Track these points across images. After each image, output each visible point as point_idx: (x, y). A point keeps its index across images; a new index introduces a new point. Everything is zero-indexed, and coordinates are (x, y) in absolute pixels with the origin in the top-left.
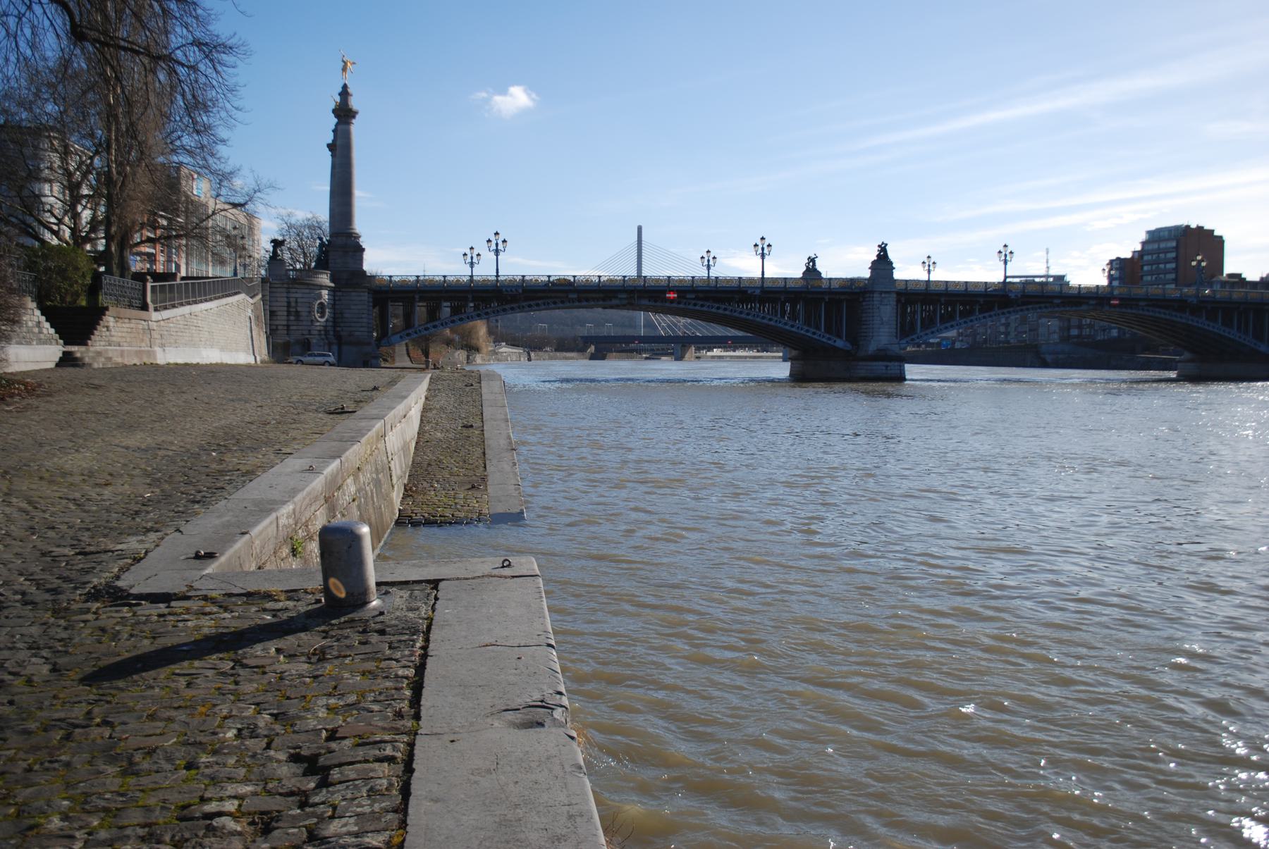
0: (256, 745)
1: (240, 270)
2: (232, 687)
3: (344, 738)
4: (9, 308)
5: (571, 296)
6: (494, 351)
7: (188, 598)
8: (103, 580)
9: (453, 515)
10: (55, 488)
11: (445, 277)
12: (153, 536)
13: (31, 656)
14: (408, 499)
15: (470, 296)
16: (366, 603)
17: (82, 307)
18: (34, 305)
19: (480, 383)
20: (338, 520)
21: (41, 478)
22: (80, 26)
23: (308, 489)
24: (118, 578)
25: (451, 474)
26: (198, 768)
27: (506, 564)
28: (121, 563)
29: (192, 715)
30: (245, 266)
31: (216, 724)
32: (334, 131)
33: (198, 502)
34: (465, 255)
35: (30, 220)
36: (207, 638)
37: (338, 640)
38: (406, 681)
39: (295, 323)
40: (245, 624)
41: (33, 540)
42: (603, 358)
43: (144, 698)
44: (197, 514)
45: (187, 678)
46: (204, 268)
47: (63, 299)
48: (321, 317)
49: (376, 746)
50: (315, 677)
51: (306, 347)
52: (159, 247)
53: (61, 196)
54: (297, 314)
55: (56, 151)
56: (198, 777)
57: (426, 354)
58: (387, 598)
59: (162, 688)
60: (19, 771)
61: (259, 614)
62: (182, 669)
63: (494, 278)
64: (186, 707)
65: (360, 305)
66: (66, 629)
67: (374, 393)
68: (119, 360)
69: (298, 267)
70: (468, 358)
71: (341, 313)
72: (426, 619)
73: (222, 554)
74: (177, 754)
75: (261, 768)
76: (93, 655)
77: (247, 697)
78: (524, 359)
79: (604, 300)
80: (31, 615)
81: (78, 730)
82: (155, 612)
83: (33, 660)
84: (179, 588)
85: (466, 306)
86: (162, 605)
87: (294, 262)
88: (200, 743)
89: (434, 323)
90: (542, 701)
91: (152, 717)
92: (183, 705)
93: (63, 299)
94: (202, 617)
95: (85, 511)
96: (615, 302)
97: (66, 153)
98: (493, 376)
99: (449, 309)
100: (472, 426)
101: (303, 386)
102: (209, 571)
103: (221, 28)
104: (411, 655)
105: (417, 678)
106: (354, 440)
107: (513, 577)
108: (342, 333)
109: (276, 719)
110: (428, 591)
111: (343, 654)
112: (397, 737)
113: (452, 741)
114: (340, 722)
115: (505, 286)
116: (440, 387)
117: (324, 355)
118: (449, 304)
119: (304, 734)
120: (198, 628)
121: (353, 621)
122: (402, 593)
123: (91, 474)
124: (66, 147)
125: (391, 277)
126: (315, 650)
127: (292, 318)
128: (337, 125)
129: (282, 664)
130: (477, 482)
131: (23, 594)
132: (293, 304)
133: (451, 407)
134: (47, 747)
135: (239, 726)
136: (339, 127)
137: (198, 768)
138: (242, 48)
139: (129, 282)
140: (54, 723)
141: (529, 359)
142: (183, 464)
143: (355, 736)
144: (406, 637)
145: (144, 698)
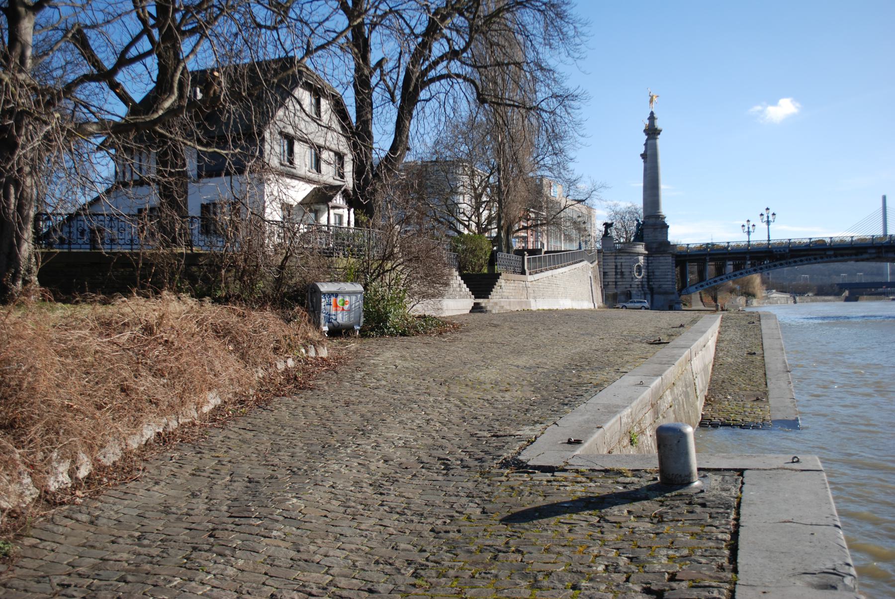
0: (620, 578)
1: (583, 245)
2: (599, 535)
3: (682, 580)
4: (444, 276)
5: (829, 253)
6: (767, 296)
7: (566, 470)
8: (510, 455)
9: (743, 420)
10: (475, 392)
11: (728, 243)
12: (539, 427)
13: (469, 502)
14: (708, 407)
15: (748, 256)
16: (690, 483)
17: (485, 274)
18: (457, 273)
19: (760, 321)
20: (664, 422)
21: (467, 385)
22: (482, 95)
23: (640, 398)
24: (519, 454)
25: (740, 389)
26: (580, 589)
27: (795, 460)
28: (521, 443)
29: (574, 552)
30: (586, 242)
31: (590, 560)
32: (646, 145)
33: (567, 404)
34: (743, 226)
35: (452, 219)
36: (580, 500)
37: (671, 508)
38: (724, 544)
39: (620, 280)
40: (604, 492)
41: (465, 426)
42: (856, 300)
43: (542, 537)
44: (567, 413)
45: (569, 526)
46: (559, 244)
47: (473, 270)
48: (639, 275)
49: (706, 589)
50: (657, 534)
51: (628, 296)
52: (529, 231)
53: (469, 203)
54: (622, 273)
55: (467, 175)
56: (581, 595)
57: (715, 300)
58: (706, 481)
59: (553, 531)
60: (467, 577)
61: (614, 485)
62: (565, 519)
63: (767, 242)
64: (569, 546)
65: (666, 266)
66: (489, 485)
67: (681, 328)
68: (508, 308)
69: (622, 241)
70: (747, 302)
71: (653, 272)
72: (736, 498)
73: (586, 441)
74: (566, 578)
75: (624, 595)
76: (507, 505)
77: (610, 543)
78: (791, 301)
79: (856, 255)
80: (467, 474)
81: (501, 554)
82: (545, 479)
83: (471, 504)
84: (559, 463)
85: (745, 263)
86: (548, 474)
87: (619, 237)
88: (581, 572)
89: (721, 277)
90: (834, 569)
91: (547, 550)
92: (568, 544)
93: (473, 270)
94: (575, 484)
95: (494, 408)
96: (865, 256)
97: (472, 175)
98: (769, 316)
99: (732, 267)
100: (754, 354)
101: (630, 324)
102: (577, 452)
103: (569, 86)
104: (727, 524)
105: (733, 542)
106: (670, 363)
107: (802, 470)
108: (654, 286)
109: (631, 561)
110: (736, 477)
111: (676, 518)
112: (721, 584)
113: (764, 593)
114: (678, 568)
115: (775, 248)
116: (729, 324)
117: (641, 302)
118: (732, 263)
119: (652, 574)
120: (574, 492)
121: (681, 495)
122: (716, 477)
123: (497, 383)
124: (473, 171)
125: (688, 245)
126: (655, 514)
127: (619, 276)
128: (647, 140)
129: (632, 522)
130: (761, 395)
131: (462, 460)
132: (619, 267)
133: (738, 339)
134: (482, 563)
135: (607, 563)
136: (649, 142)
137: (580, 589)
138: (584, 96)
139: (513, 256)
140: (485, 547)
141: (795, 302)
142: (554, 378)
143: (690, 580)
144: (722, 510)
145: (542, 537)
